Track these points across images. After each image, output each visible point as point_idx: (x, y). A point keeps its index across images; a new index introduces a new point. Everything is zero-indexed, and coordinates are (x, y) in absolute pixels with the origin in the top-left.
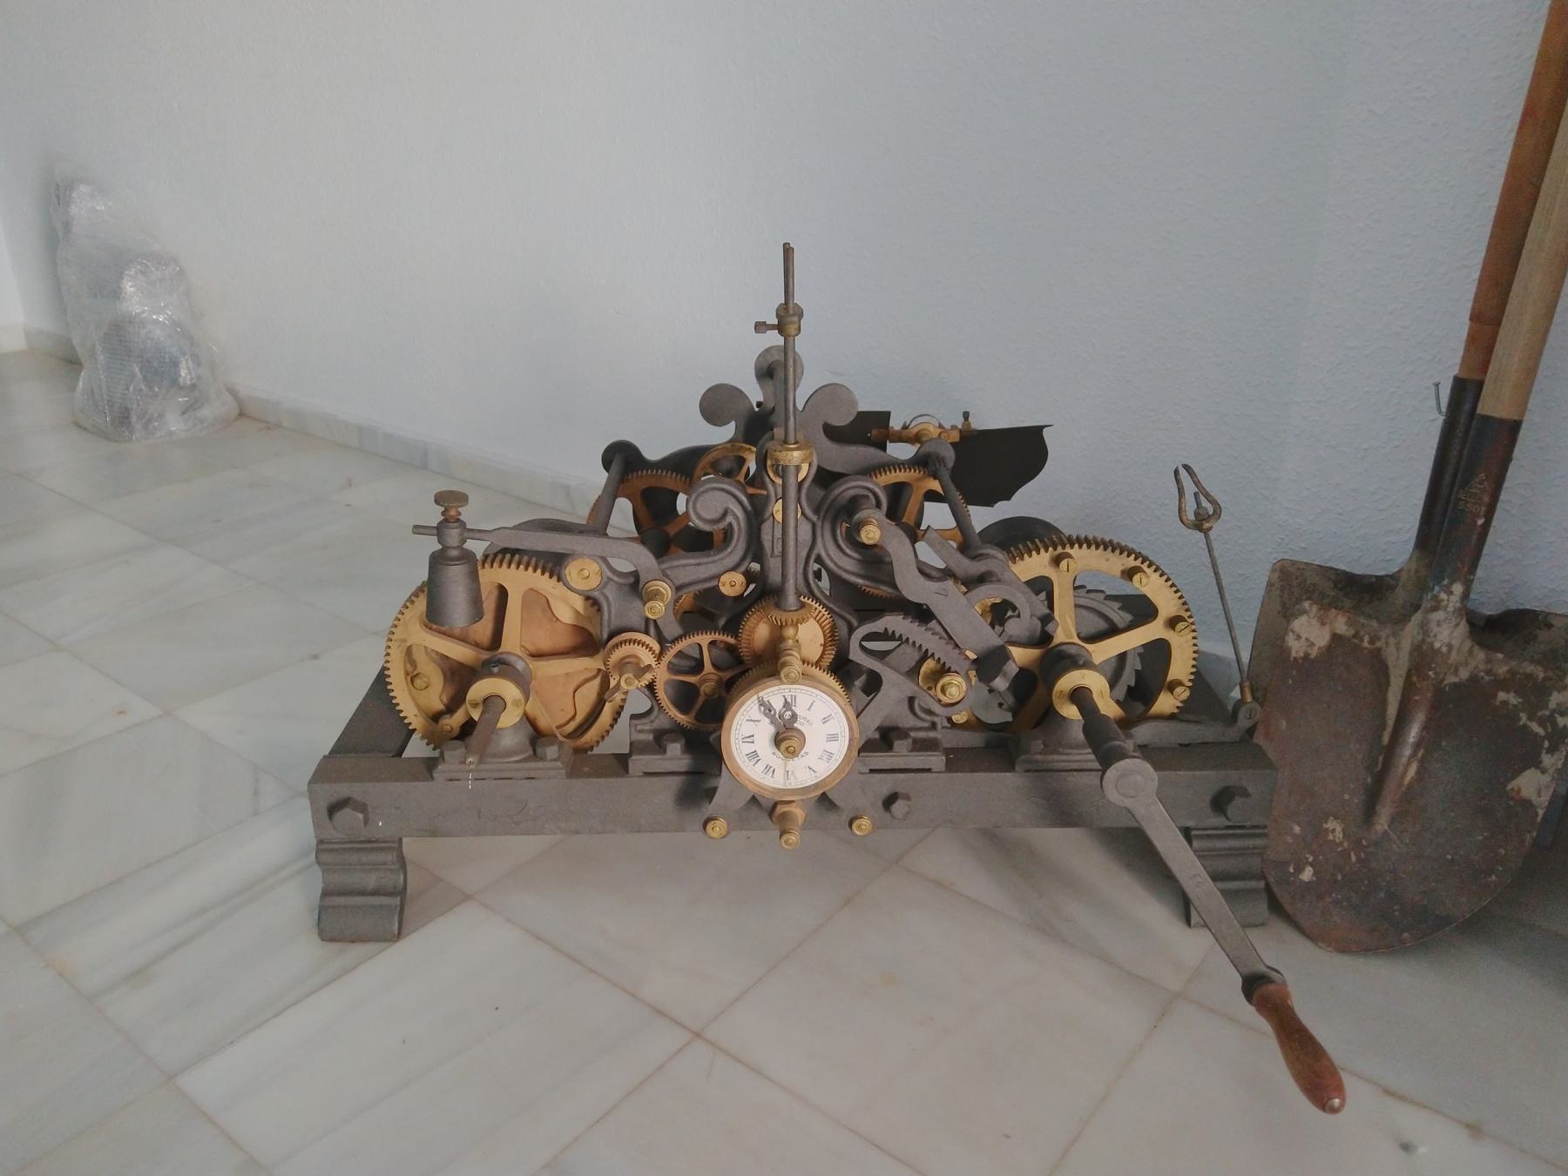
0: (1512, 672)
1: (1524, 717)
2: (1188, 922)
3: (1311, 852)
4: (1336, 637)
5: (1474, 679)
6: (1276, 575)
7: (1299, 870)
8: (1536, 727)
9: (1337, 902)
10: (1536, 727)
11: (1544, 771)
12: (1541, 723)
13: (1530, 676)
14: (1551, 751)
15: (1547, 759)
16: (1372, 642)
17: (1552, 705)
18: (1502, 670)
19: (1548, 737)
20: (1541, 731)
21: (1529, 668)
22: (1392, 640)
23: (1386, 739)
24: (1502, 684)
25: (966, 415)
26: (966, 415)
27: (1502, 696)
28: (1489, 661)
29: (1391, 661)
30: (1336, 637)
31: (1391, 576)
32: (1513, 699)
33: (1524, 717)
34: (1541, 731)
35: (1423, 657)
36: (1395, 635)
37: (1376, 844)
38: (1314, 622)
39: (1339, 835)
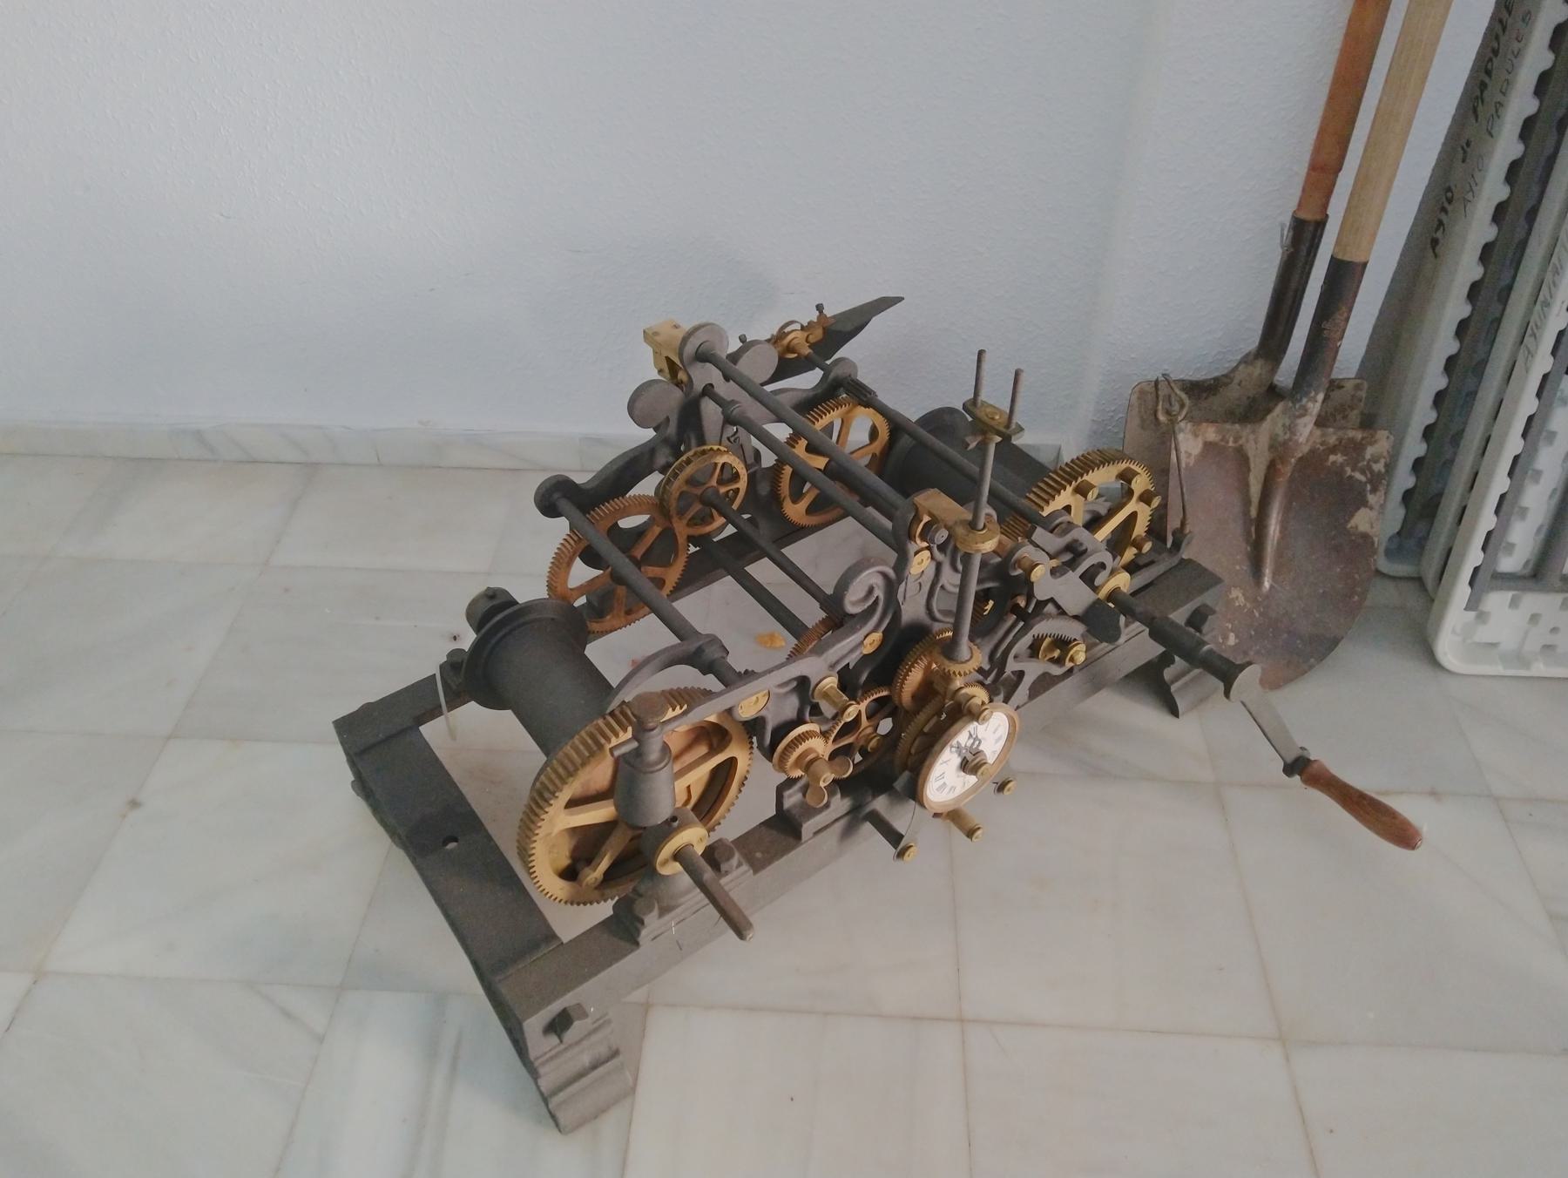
0: (1340, 440)
1: (1348, 470)
2: (1174, 712)
3: (1229, 621)
4: (1208, 445)
5: (1313, 451)
6: (1134, 397)
7: (1226, 638)
8: (1358, 476)
9: (1258, 652)
10: (1358, 476)
11: (1371, 508)
12: (1363, 472)
13: (1352, 440)
14: (1374, 490)
15: (1371, 499)
16: (1235, 441)
17: (1368, 456)
18: (1332, 440)
19: (1370, 481)
20: (1363, 478)
21: (1351, 434)
22: (1252, 437)
23: (1254, 513)
24: (1333, 450)
25: (820, 308)
26: (820, 308)
27: (1332, 458)
28: (1323, 435)
29: (1251, 454)
30: (1208, 445)
31: (1225, 376)
32: (1337, 458)
33: (1348, 470)
34: (1363, 478)
35: (1279, 450)
36: (1253, 432)
37: (1267, 597)
38: (1190, 436)
39: (1242, 599)
